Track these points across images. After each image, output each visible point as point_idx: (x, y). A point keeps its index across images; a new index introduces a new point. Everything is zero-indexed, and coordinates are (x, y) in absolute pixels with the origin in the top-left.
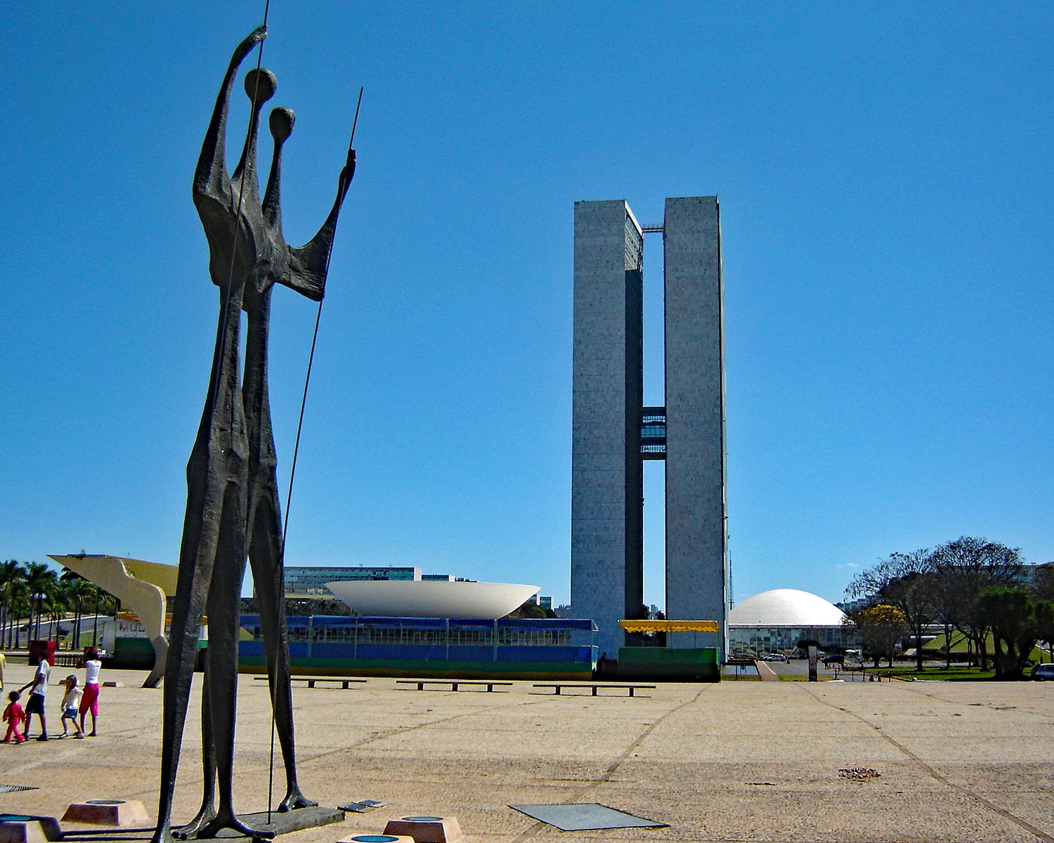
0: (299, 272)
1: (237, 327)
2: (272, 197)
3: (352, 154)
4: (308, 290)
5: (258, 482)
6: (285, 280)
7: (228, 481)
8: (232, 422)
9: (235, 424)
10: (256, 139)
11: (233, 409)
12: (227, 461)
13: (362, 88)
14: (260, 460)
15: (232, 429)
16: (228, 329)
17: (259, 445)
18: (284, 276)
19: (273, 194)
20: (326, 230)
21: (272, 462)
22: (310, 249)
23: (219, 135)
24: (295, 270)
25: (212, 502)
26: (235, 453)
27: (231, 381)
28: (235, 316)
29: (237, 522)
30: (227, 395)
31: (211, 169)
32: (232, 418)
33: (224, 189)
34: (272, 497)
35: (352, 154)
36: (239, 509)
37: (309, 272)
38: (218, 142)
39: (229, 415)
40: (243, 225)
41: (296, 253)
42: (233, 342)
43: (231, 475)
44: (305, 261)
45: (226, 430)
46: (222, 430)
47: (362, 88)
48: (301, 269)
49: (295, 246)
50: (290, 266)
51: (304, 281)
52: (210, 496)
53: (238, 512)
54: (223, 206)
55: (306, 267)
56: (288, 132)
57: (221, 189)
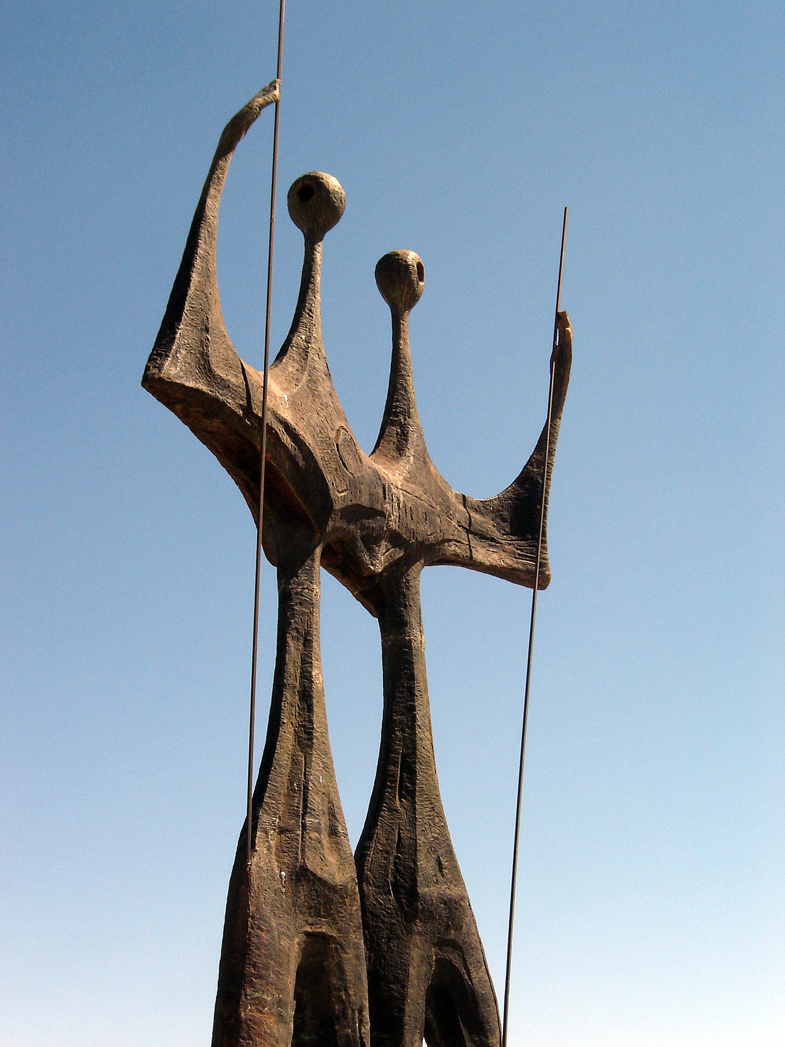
0: (493, 540)
1: (308, 633)
2: (397, 407)
3: (561, 320)
4: (514, 569)
5: (420, 934)
6: (457, 555)
7: (307, 934)
8: (305, 813)
9: (312, 816)
10: (314, 293)
11: (306, 788)
12: (296, 893)
13: (566, 208)
14: (422, 890)
15: (304, 826)
16: (289, 640)
17: (415, 862)
18: (453, 548)
19: (397, 401)
20: (537, 460)
21: (448, 892)
22: (510, 499)
23: (194, 275)
24: (483, 537)
25: (260, 977)
26: (314, 875)
27: (303, 735)
28: (303, 614)
29: (345, 1015)
30: (295, 762)
31: (176, 333)
32: (305, 807)
33: (219, 372)
34: (465, 961)
35: (561, 320)
36: (346, 990)
37: (513, 538)
38: (192, 287)
39: (298, 801)
40: (286, 439)
41: (483, 508)
42: (304, 662)
43: (310, 920)
44: (504, 520)
45: (290, 831)
46: (282, 831)
47: (566, 208)
48: (496, 534)
49: (476, 497)
50: (468, 532)
51: (503, 554)
52: (254, 965)
53: (343, 994)
54: (223, 405)
55: (507, 529)
56: (413, 298)
57: (210, 370)
